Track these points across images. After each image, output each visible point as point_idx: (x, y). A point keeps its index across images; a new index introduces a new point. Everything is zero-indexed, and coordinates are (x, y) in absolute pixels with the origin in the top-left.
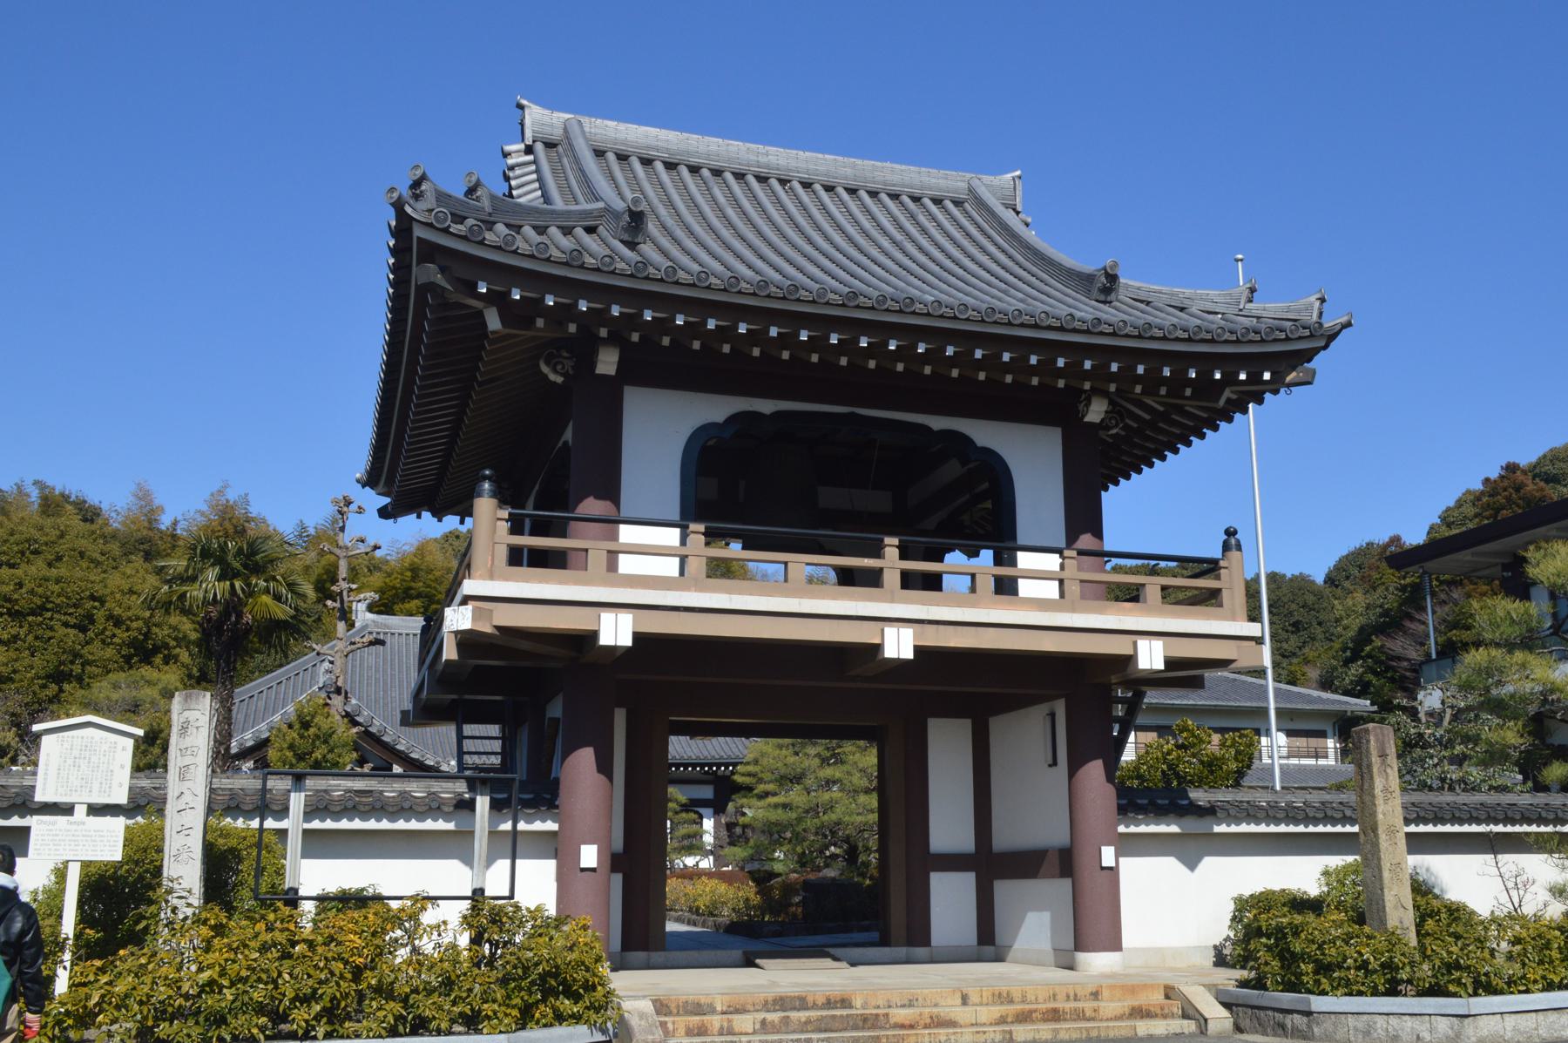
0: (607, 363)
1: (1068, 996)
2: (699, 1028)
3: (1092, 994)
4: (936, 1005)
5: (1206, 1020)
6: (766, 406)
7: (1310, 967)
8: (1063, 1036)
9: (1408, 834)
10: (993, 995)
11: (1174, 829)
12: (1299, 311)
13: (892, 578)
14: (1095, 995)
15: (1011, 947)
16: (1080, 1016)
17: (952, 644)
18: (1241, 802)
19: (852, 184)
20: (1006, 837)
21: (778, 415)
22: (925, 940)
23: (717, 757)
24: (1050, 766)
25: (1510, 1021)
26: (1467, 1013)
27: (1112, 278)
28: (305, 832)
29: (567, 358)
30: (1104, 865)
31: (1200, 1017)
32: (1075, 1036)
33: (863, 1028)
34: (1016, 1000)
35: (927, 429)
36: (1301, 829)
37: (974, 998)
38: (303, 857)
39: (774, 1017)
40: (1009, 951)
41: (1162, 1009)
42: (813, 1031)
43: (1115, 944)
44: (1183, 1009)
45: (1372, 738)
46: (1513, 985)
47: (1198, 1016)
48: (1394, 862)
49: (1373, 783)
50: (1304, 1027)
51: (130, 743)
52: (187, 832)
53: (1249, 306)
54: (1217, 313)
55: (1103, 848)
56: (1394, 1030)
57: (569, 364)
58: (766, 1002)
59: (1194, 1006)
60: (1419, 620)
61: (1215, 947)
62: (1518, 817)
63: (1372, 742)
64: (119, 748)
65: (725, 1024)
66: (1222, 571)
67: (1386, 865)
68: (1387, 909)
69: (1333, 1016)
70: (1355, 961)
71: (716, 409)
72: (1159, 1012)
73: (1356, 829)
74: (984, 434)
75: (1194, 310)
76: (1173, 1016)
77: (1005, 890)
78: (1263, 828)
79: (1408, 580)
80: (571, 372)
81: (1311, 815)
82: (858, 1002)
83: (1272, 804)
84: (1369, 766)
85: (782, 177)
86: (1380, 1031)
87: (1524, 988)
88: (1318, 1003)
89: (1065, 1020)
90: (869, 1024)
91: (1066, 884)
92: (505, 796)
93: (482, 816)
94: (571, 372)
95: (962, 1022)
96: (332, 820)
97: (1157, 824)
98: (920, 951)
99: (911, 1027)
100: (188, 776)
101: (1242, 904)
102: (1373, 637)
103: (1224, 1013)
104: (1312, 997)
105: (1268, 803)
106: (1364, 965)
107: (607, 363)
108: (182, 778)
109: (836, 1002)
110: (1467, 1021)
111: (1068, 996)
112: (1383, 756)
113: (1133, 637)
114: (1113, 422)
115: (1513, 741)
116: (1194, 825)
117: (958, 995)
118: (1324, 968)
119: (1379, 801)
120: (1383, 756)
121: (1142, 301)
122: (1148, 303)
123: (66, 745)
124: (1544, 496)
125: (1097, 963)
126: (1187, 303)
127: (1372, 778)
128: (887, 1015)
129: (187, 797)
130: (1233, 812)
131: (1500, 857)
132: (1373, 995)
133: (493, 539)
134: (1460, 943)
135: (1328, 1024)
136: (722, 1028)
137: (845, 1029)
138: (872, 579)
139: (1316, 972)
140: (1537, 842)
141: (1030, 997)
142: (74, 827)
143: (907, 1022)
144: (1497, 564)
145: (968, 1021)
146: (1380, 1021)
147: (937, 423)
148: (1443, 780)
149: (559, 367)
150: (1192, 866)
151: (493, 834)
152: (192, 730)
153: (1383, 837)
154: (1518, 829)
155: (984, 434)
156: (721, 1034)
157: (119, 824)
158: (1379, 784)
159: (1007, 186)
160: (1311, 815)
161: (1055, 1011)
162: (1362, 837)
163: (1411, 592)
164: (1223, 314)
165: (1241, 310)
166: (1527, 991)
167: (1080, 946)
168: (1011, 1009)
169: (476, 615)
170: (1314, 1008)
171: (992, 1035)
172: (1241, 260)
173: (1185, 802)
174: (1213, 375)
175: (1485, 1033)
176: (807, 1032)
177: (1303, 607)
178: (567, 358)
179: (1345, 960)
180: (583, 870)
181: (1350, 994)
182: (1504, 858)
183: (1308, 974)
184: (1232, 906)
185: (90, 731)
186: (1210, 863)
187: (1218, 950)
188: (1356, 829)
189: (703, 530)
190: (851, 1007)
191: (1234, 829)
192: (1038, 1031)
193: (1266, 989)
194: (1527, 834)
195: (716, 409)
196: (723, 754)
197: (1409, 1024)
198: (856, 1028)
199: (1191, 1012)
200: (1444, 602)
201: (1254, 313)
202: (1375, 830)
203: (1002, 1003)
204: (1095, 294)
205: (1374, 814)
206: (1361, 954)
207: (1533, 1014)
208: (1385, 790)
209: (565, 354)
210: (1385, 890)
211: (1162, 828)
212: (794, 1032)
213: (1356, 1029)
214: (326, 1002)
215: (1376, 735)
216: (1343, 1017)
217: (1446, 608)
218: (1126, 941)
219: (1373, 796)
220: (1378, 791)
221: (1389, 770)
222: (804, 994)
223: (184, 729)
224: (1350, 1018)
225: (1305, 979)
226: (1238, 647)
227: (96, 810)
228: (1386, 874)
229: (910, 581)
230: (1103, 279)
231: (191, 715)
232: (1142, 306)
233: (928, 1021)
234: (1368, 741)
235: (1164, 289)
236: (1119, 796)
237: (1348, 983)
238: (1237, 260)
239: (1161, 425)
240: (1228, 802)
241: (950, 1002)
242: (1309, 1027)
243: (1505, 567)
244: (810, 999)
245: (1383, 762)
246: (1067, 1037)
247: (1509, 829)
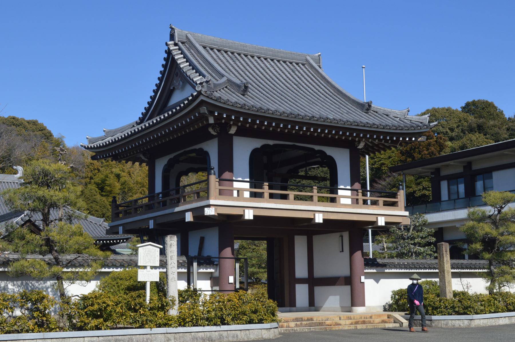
0: (233, 130)
1: (364, 318)
2: (281, 326)
3: (370, 317)
4: (333, 320)
5: (402, 323)
6: (271, 142)
7: (431, 308)
8: (369, 327)
9: (452, 273)
10: (347, 317)
11: (375, 271)
12: (423, 120)
13: (315, 199)
14: (371, 317)
15: (322, 307)
16: (370, 322)
17: (331, 218)
18: (391, 263)
19: (272, 57)
20: (318, 273)
21: (275, 145)
22: (295, 306)
23: (99, 237)
24: (341, 252)
25: (482, 321)
26: (472, 319)
27: (370, 106)
28: (178, 273)
30: (230, 282)
31: (399, 322)
32: (371, 327)
33: (319, 326)
34: (352, 319)
35: (313, 149)
36: (408, 271)
37: (342, 318)
38: (198, 280)
39: (298, 323)
40: (321, 308)
41: (389, 321)
42: (308, 327)
43: (363, 305)
44: (394, 320)
45: (444, 246)
46: (482, 312)
47: (399, 322)
48: (448, 280)
49: (444, 259)
50: (430, 324)
51: (159, 249)
52: (173, 273)
53: (408, 116)
54: (398, 118)
55: (230, 277)
56: (454, 324)
57: (218, 129)
58: (293, 319)
59: (400, 321)
60: (380, 183)
61: (383, 306)
62: (465, 267)
63: (444, 248)
64: (156, 250)
65: (287, 325)
66: (398, 196)
67: (447, 281)
68: (447, 293)
69: (438, 321)
70: (444, 306)
71: (257, 143)
72: (388, 321)
73: (437, 271)
74: (330, 151)
75: (391, 116)
76: (392, 322)
77: (318, 290)
78: (398, 271)
79: (376, 166)
80: (219, 132)
81: (411, 267)
82: (315, 319)
83: (399, 263)
84: (443, 254)
85: (252, 55)
86: (450, 324)
87: (485, 313)
88: (434, 317)
89: (366, 324)
90: (321, 324)
91: (348, 288)
93: (238, 269)
94: (219, 132)
95: (342, 324)
96: (184, 269)
97: (370, 269)
98: (294, 308)
99: (331, 325)
100: (173, 258)
101: (395, 293)
103: (406, 321)
104: (432, 316)
105: (398, 263)
106: (446, 307)
107: (233, 130)
108: (171, 259)
109: (310, 319)
110: (472, 321)
111: (364, 318)
112: (446, 251)
113: (377, 216)
115: (479, 248)
116: (380, 270)
117: (339, 317)
118: (435, 308)
119: (445, 264)
120: (446, 251)
121: (374, 111)
122: (377, 112)
123: (145, 250)
124: (430, 135)
125: (359, 310)
126: (389, 114)
127: (443, 257)
128: (325, 322)
129: (173, 264)
130: (391, 266)
131: (462, 279)
132: (448, 315)
134: (470, 301)
135: (436, 323)
136: (287, 326)
137: (315, 326)
138: (310, 198)
139: (432, 310)
140: (477, 274)
141: (356, 318)
142: (148, 272)
143: (329, 324)
144: (429, 172)
145: (344, 324)
146: (450, 322)
147: (317, 148)
148: (409, 252)
149: (216, 130)
150: (377, 282)
151: (198, 273)
152: (172, 246)
153: (446, 274)
154: (473, 271)
155: (330, 151)
156: (287, 327)
157: (158, 271)
158: (445, 259)
159: (317, 59)
160: (411, 267)
161: (364, 321)
162: (440, 273)
163: (376, 171)
164: (400, 118)
165: (405, 118)
166: (486, 313)
167: (353, 304)
168: (354, 321)
169: (216, 210)
170: (433, 319)
171: (352, 327)
172: (364, 68)
173: (376, 263)
174: (400, 139)
175: (476, 324)
176: (306, 327)
177: (322, 172)
178: (217, 127)
179: (441, 306)
180: (229, 283)
181: (442, 315)
182: (463, 279)
183: (430, 310)
184: (391, 294)
185: (150, 246)
186: (382, 281)
187: (384, 307)
188: (437, 271)
189: (268, 184)
190: (313, 321)
191: (390, 271)
192: (363, 326)
193: (417, 315)
194: (476, 272)
195: (257, 143)
196: (98, 235)
197: (457, 322)
198: (318, 326)
199: (397, 321)
200: (390, 176)
201: (409, 119)
202: (444, 271)
203: (349, 319)
204: (364, 110)
205: (444, 268)
206: (445, 304)
207: (487, 319)
208: (447, 261)
209: (217, 126)
210: (446, 288)
211: (372, 271)
212: (303, 327)
213: (444, 324)
214: (233, 315)
215: (445, 246)
216: (440, 321)
217: (390, 179)
218: (366, 305)
219: (444, 263)
220: (445, 261)
221: (448, 255)
222: (302, 317)
223: (171, 246)
224: (442, 321)
225: (429, 311)
226: (403, 219)
228: (447, 284)
229: (321, 200)
230: (367, 106)
231: (172, 242)
232: (375, 113)
233: (335, 324)
234: (443, 247)
235: (382, 108)
236: (364, 261)
237: (442, 312)
238: (363, 68)
239: (375, 148)
240: (387, 263)
241: (337, 319)
242: (431, 324)
243: (432, 173)
244: (303, 318)
245: (446, 253)
246: (369, 328)
247: (471, 271)
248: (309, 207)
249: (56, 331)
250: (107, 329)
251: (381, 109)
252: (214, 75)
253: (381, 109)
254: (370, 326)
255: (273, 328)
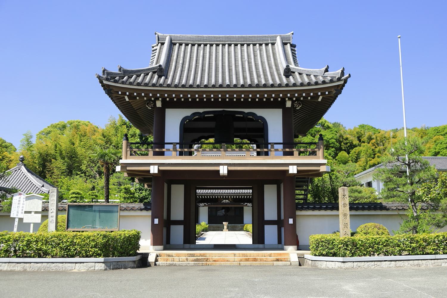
6: (201, 110)
29: (152, 103)
35: (244, 112)
71: (188, 112)
74: (259, 112)
92: (150, 207)
102: (136, 180)
107: (159, 104)
114: (298, 106)
133: (127, 150)
147: (246, 111)
149: (150, 106)
155: (259, 112)
172: (400, 37)
178: (152, 103)
195: (188, 112)
209: (151, 102)
227: (36, 212)
248: (170, 160)
249: (97, 257)
250: (362, 255)
251: (305, 71)
252: (174, 64)
253: (305, 71)
254: (191, 263)
255: (341, 262)
